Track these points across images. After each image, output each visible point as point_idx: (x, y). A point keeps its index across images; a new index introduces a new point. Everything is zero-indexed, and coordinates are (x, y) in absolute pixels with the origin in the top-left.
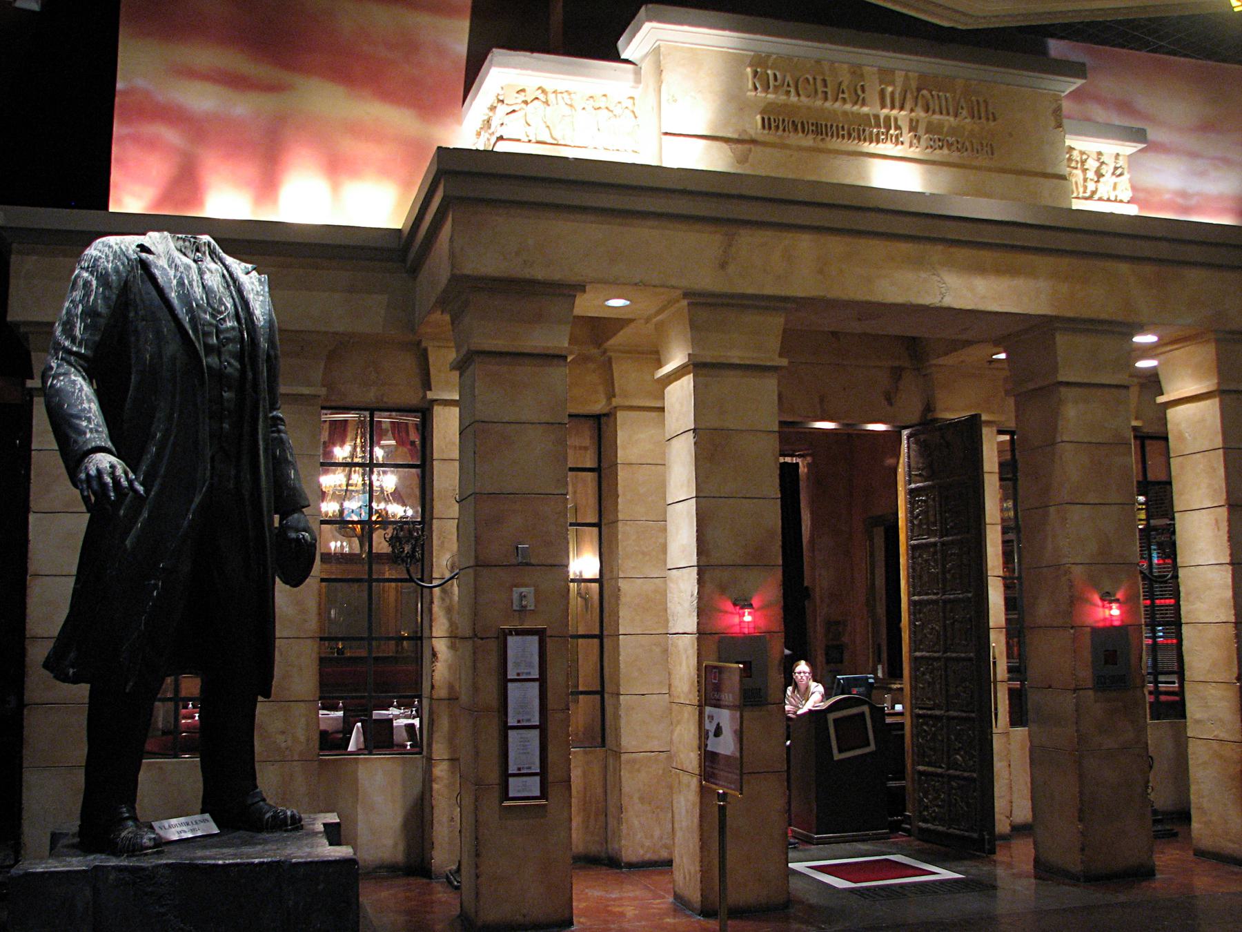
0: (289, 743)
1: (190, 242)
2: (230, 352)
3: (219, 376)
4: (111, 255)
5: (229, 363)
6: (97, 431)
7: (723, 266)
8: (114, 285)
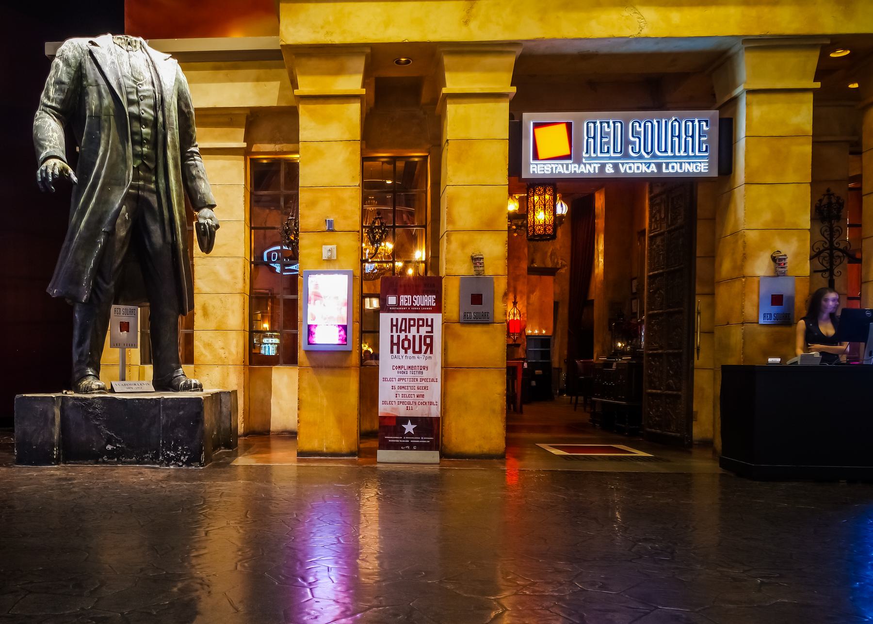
0: (227, 354)
1: (124, 39)
2: (147, 105)
3: (138, 118)
4: (72, 48)
5: (145, 111)
6: (54, 147)
7: (466, 23)
8: (73, 65)
